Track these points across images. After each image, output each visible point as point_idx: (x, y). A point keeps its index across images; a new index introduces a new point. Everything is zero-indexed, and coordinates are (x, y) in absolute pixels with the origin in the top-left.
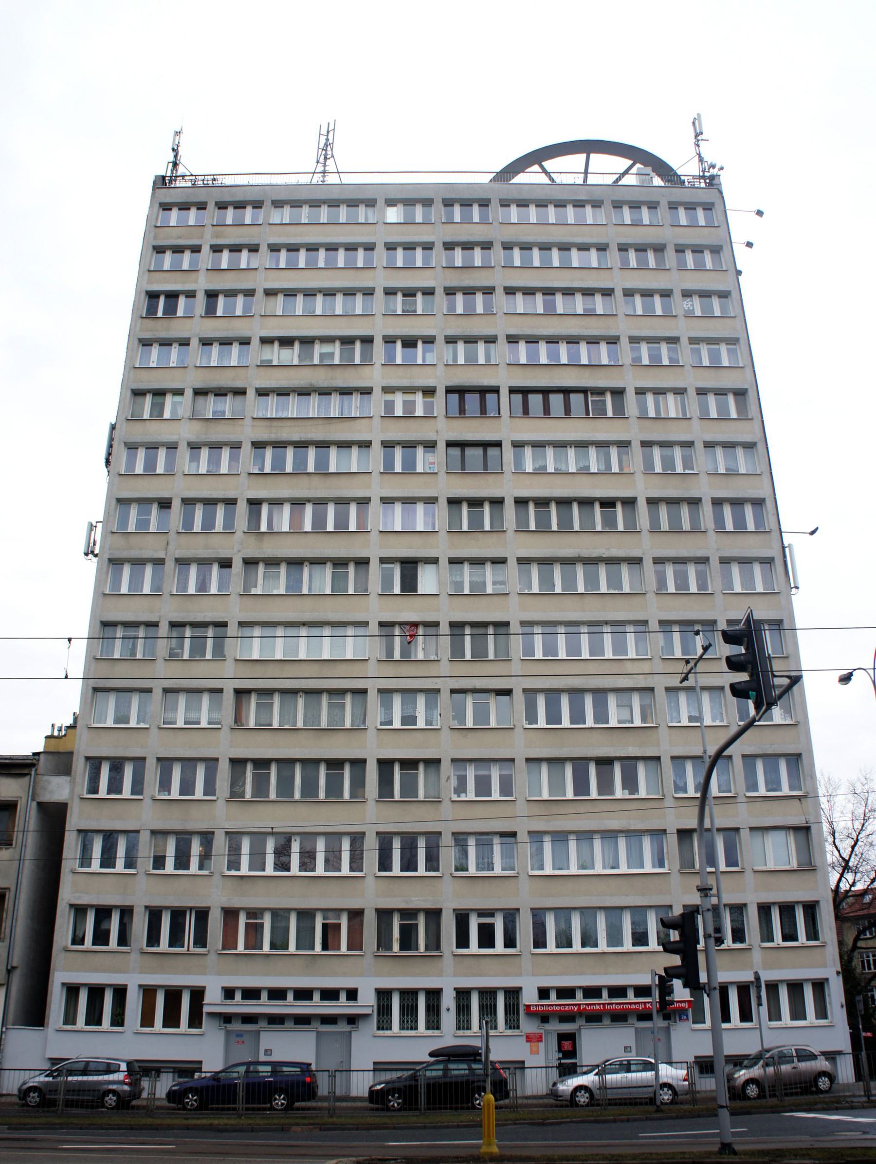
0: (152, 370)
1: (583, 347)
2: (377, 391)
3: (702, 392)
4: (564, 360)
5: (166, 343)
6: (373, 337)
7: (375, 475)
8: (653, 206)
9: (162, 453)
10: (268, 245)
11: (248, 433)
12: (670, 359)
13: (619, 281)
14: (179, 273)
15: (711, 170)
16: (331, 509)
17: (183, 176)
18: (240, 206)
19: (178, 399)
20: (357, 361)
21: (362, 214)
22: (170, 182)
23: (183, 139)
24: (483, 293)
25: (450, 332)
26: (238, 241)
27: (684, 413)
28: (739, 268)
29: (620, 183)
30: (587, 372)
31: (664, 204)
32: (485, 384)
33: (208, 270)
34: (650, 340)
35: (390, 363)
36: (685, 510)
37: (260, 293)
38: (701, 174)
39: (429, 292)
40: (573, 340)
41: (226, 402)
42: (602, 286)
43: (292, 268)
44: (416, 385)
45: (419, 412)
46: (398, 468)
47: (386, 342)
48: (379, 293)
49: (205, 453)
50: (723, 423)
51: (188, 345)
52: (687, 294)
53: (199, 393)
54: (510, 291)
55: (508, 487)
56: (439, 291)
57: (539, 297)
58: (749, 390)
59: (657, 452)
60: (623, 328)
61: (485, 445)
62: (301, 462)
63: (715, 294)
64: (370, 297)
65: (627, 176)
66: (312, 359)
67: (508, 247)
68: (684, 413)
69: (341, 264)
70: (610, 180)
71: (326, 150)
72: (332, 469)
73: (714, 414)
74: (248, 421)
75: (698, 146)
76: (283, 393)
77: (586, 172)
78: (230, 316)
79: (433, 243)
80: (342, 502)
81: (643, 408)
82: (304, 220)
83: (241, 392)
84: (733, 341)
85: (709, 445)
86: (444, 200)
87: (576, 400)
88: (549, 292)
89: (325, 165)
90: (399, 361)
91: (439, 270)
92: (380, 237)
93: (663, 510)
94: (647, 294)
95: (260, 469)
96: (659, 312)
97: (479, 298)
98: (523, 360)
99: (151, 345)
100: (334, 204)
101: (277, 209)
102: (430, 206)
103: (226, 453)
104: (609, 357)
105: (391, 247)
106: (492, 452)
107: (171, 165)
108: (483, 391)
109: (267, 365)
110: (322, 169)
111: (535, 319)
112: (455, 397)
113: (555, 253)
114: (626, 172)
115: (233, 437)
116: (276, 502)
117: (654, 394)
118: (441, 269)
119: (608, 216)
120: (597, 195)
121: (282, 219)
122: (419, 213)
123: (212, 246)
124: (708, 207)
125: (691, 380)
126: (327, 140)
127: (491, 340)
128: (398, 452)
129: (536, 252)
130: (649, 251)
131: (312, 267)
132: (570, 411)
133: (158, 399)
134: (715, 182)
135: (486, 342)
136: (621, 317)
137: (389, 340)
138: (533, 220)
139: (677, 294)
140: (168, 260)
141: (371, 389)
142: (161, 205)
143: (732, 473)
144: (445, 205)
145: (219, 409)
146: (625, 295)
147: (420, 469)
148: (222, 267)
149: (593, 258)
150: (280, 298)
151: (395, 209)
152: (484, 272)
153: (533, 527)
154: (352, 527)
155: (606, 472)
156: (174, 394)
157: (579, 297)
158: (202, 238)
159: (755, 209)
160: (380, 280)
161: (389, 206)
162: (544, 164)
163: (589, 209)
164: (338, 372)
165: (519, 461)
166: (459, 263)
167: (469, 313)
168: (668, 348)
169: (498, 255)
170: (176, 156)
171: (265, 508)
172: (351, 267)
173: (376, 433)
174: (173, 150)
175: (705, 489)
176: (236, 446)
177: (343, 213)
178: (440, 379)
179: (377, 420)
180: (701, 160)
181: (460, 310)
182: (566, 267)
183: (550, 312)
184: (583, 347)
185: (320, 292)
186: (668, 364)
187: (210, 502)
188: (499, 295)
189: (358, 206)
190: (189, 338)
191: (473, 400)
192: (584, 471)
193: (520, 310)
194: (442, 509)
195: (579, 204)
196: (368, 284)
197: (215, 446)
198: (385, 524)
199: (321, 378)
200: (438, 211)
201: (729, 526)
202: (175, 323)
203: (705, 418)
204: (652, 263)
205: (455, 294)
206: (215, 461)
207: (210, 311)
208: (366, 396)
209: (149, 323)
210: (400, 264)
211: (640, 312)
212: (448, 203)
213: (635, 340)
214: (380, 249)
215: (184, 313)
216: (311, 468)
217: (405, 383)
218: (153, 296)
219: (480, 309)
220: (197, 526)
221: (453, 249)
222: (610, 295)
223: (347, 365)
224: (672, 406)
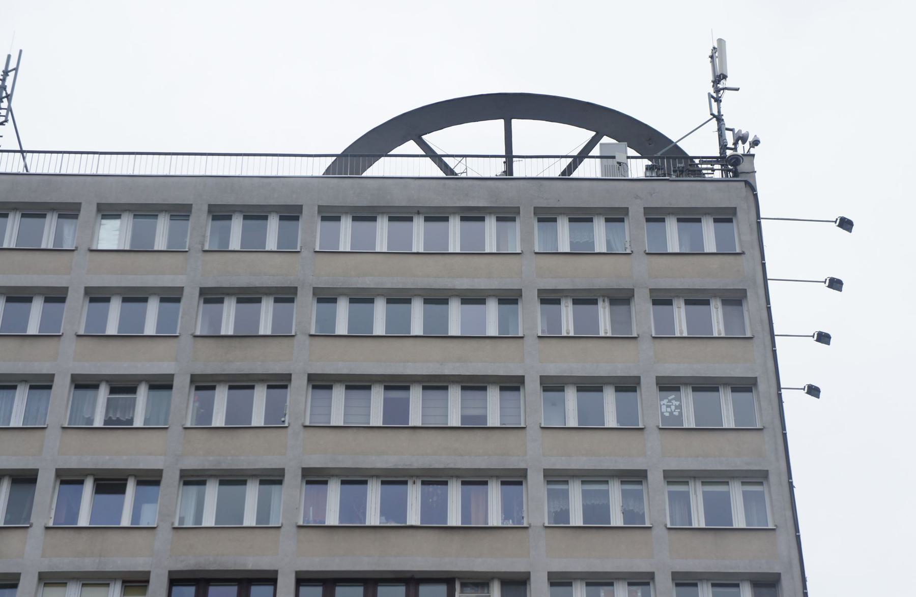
6: (36, 472)
8: (616, 216)
13: (533, 363)
25: (192, 463)
29: (575, 175)
32: (250, 567)
34: (589, 477)
40: (434, 479)
42: (502, 373)
47: (63, 482)
52: (668, 385)
56: (182, 383)
60: (535, 454)
64: (45, 392)
65: (586, 161)
67: (662, 299)
70: (555, 169)
75: (718, 100)
77: (509, 157)
79: (181, 289)
88: (397, 384)
90: (83, 520)
92: (77, 277)
94: (590, 386)
111: (362, 436)
114: (584, 154)
119: (527, 238)
122: (162, 228)
130: (600, 303)
135: (262, 482)
136: (533, 432)
137: (70, 479)
148: (108, 333)
151: (116, 223)
152: (275, 347)
157: (455, 395)
160: (66, 360)
161: (105, 217)
162: (426, 138)
167: (237, 425)
188: (298, 395)
212: (221, 214)
217: (89, 564)
219: (258, 419)
221: (221, 301)
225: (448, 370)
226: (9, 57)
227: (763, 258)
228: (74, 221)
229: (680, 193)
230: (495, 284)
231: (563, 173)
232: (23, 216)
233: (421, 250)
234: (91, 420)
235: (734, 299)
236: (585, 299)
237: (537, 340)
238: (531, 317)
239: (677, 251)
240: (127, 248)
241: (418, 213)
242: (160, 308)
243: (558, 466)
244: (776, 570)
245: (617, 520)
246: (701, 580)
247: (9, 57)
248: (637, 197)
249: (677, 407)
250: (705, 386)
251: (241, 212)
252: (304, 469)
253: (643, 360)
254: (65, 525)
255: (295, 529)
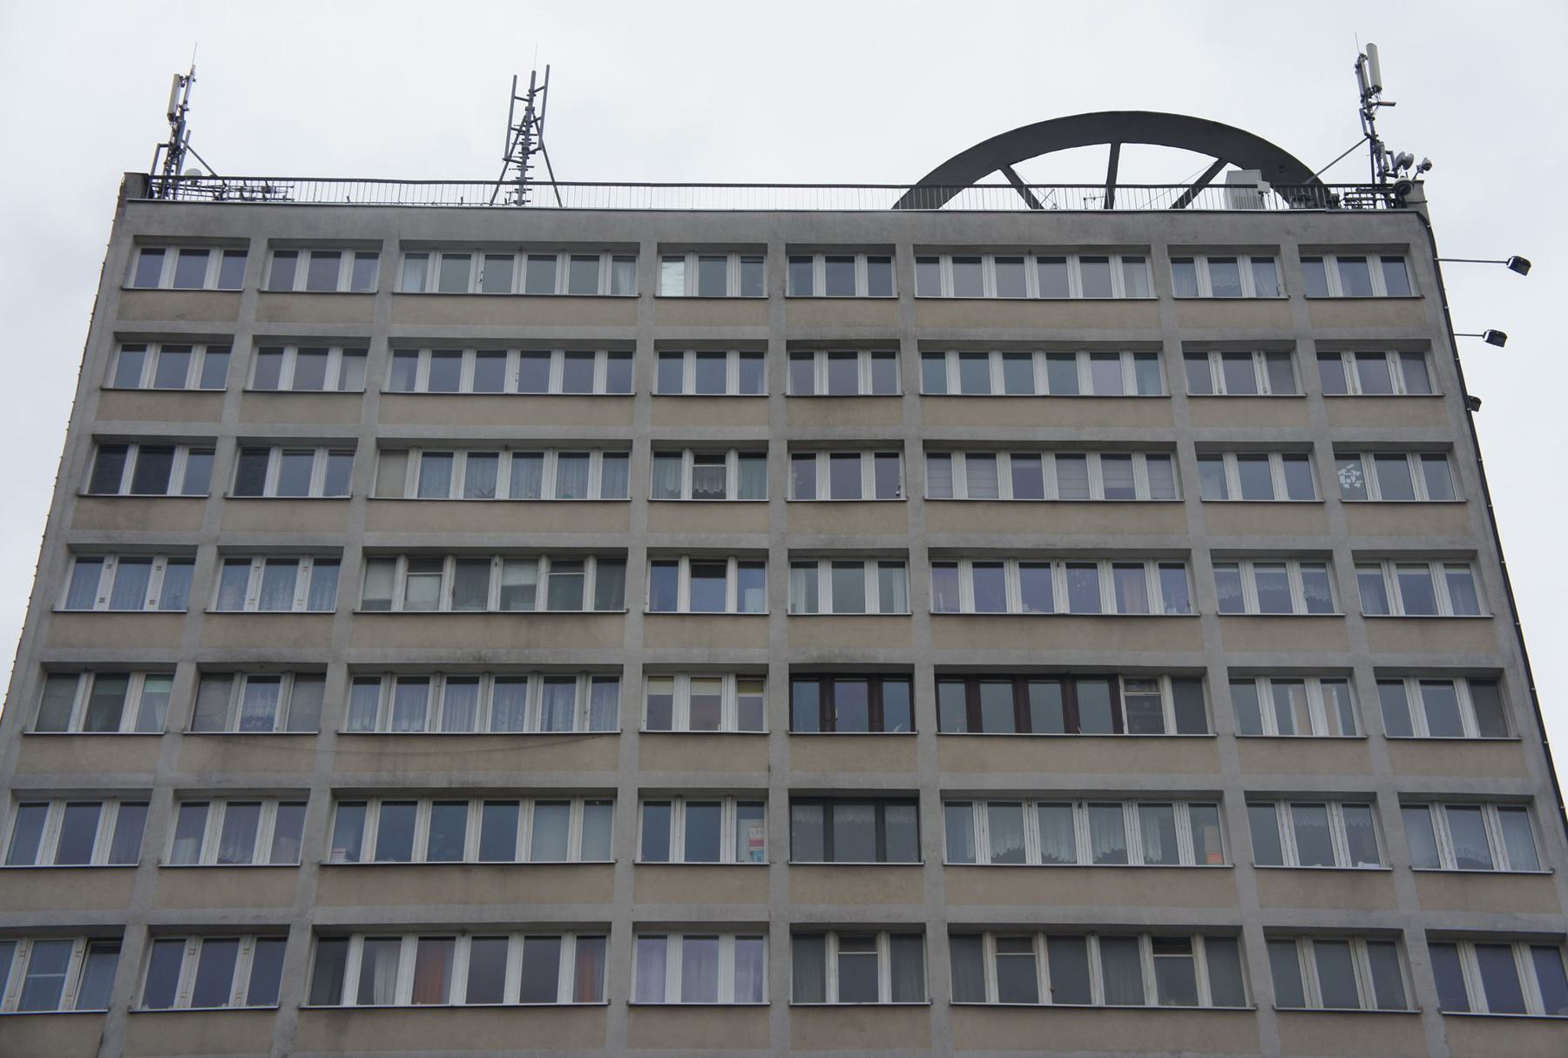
1: (1106, 577)
2: (632, 675)
3: (1389, 677)
4: (1062, 605)
5: (136, 557)
7: (623, 872)
9: (108, 820)
10: (390, 339)
12: (1310, 602)
13: (1187, 427)
14: (177, 397)
15: (1401, 172)
16: (515, 953)
17: (195, 178)
18: (326, 251)
19: (158, 687)
20: (588, 605)
21: (605, 275)
22: (163, 190)
24: (878, 456)
25: (802, 542)
29: (1189, 207)
30: (1116, 632)
31: (1290, 251)
32: (881, 660)
33: (245, 392)
35: (663, 610)
36: (1362, 961)
37: (367, 449)
38: (1378, 181)
39: (754, 452)
40: (1081, 561)
41: (275, 696)
42: (1148, 438)
45: (729, 724)
46: (677, 855)
47: (655, 564)
48: (641, 455)
49: (216, 817)
50: (1446, 750)
51: (192, 562)
52: (1347, 452)
53: (211, 674)
54: (938, 451)
55: (932, 899)
56: (778, 451)
57: (1004, 465)
58: (1507, 673)
59: (1286, 820)
60: (1198, 532)
61: (881, 800)
62: (447, 840)
63: (1414, 452)
64: (620, 461)
66: (484, 600)
67: (933, 351)
68: (1348, 724)
70: (1165, 200)
71: (527, 134)
72: (522, 855)
74: (326, 741)
75: (1370, 118)
76: (413, 676)
77: (1111, 185)
80: (542, 935)
81: (1250, 714)
82: (474, 287)
83: (313, 674)
85: (1413, 802)
86: (790, 248)
87: (1092, 695)
88: (1026, 451)
89: (523, 167)
90: (683, 606)
91: (777, 402)
92: (646, 329)
93: (1308, 961)
94: (1253, 453)
95: (349, 856)
96: (1281, 494)
97: (868, 466)
98: (968, 606)
99: (100, 561)
100: (542, 252)
101: (412, 262)
102: (760, 260)
103: (267, 819)
105: (669, 351)
106: (897, 817)
107: (164, 152)
108: (877, 677)
109: (377, 611)
110: (518, 174)
111: (994, 511)
112: (812, 689)
114: (1204, 182)
116: (384, 936)
117: (1274, 682)
118: (782, 401)
121: (423, 287)
122: (734, 276)
123: (257, 340)
124: (1394, 255)
125: (1363, 650)
126: (530, 110)
127: (894, 560)
128: (678, 820)
129: (996, 364)
130: (1255, 358)
133: (108, 688)
134: (1409, 197)
136: (1193, 507)
137: (663, 560)
138: (991, 291)
139: (1324, 453)
140: (149, 368)
143: (1474, 873)
144: (793, 260)
145: (259, 712)
146: (1200, 458)
147: (727, 856)
149: (1127, 375)
150: (415, 460)
151: (680, 266)
152: (879, 408)
153: (993, 998)
154: (565, 996)
155: (1166, 867)
157: (1094, 464)
158: (235, 319)
159: (1509, 255)
160: (643, 425)
161: (666, 259)
163: (1116, 267)
165: (959, 840)
168: (1305, 576)
170: (177, 133)
171: (355, 953)
173: (628, 769)
174: (172, 117)
175: (1410, 910)
176: (293, 800)
177: (563, 274)
178: (776, 648)
179: (629, 742)
180: (1377, 149)
181: (823, 493)
182: (1064, 396)
185: (507, 448)
186: (1305, 612)
187: (220, 937)
188: (914, 464)
190: (195, 547)
192: (1113, 864)
193: (961, 493)
194: (778, 952)
195: (1094, 256)
197: (244, 801)
198: (643, 988)
199: (503, 644)
200: (776, 273)
201: (1479, 1003)
202: (159, 511)
203: (1400, 738)
204: (1263, 385)
205: (813, 457)
207: (249, 486)
208: (606, 686)
211: (1236, 494)
212: (800, 255)
213: (1225, 559)
216: (471, 854)
217: (698, 656)
218: (109, 449)
219: (869, 492)
220: (184, 996)
222: (1167, 458)
223: (566, 612)
224: (1318, 711)
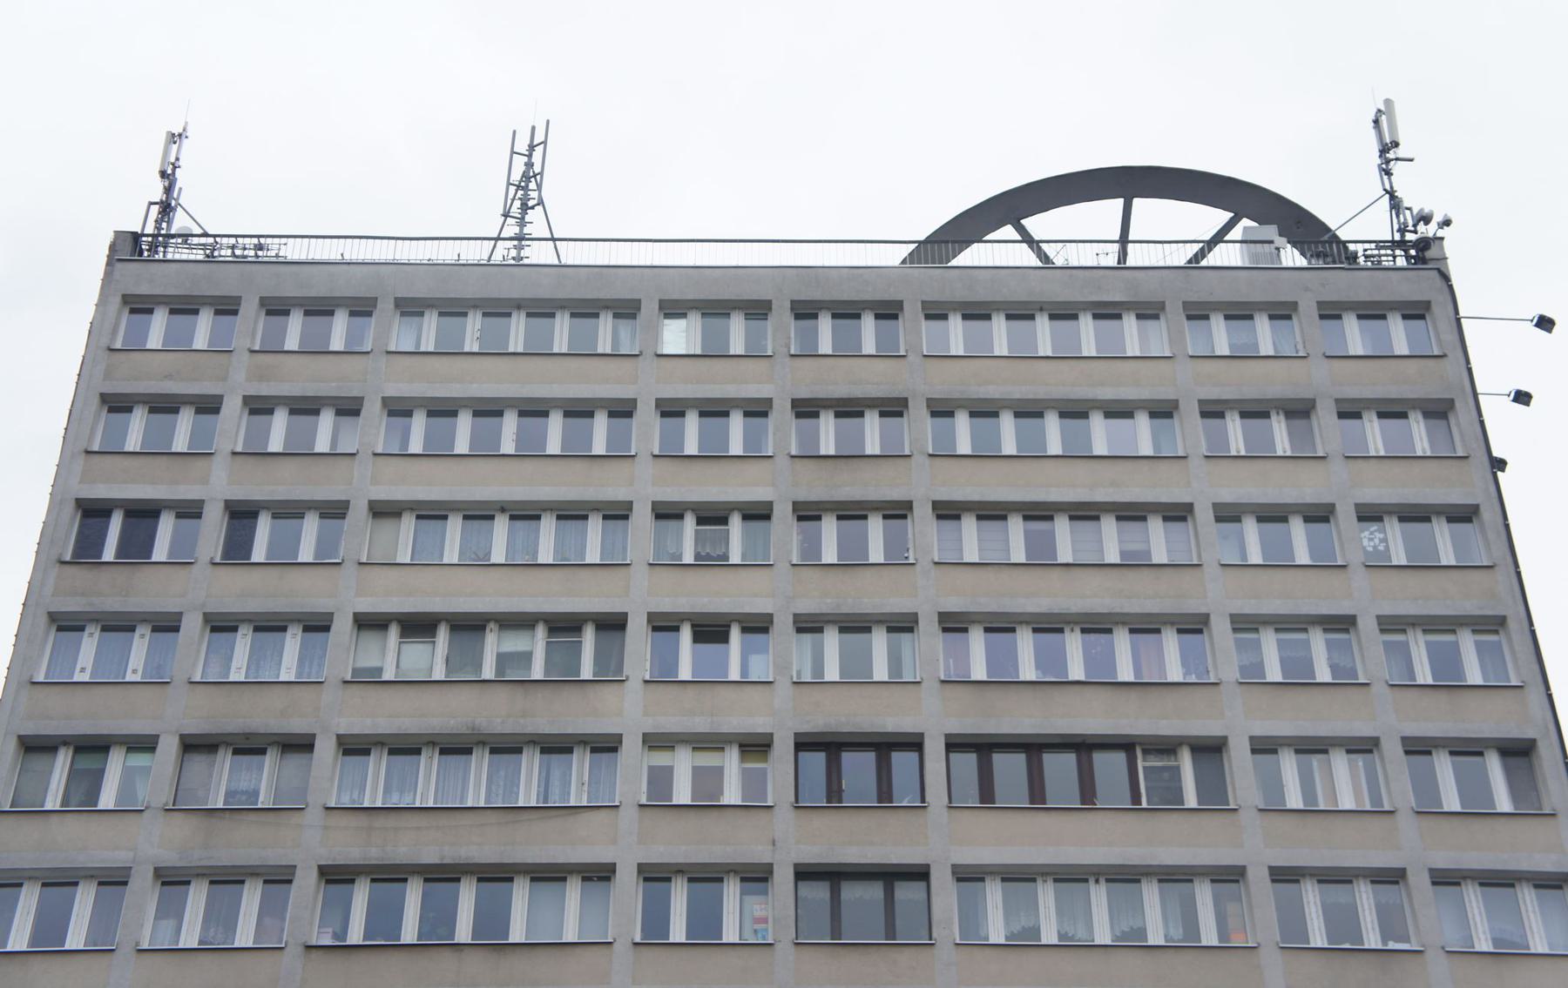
0: (79, 690)
2: (631, 746)
3: (1417, 748)
4: (1076, 672)
5: (119, 625)
8: (1282, 312)
9: (84, 900)
11: (310, 844)
12: (1334, 668)
13: (1204, 488)
15: (1421, 227)
17: (186, 236)
18: (319, 309)
20: (587, 672)
22: (153, 248)
23: (188, 153)
25: (807, 606)
26: (311, 390)
27: (1375, 796)
28: (1496, 453)
29: (1204, 263)
31: (1308, 308)
33: (234, 453)
37: (359, 512)
38: (1397, 237)
39: (758, 514)
40: (1096, 626)
41: (261, 768)
43: (438, 453)
44: (725, 729)
46: (678, 933)
47: (655, 629)
48: (642, 516)
49: (197, 897)
50: (1477, 825)
51: (176, 629)
52: (1369, 514)
53: (194, 746)
54: (948, 512)
56: (783, 512)
59: (1311, 896)
60: (1218, 597)
61: (890, 876)
62: (439, 918)
64: (620, 523)
67: (942, 410)
68: (1375, 796)
69: (554, 447)
70: (1181, 256)
71: (526, 190)
72: (517, 935)
73: (1451, 801)
74: (314, 816)
75: (1388, 173)
76: (405, 747)
77: (1124, 240)
78: (283, 562)
79: (769, 401)
81: (1274, 786)
82: (471, 345)
83: (300, 745)
84: (1491, 625)
85: (1445, 879)
88: (1038, 513)
89: (522, 223)
90: (685, 673)
91: (782, 462)
92: (646, 387)
94: (1272, 515)
95: (335, 936)
96: (1302, 557)
97: (875, 527)
100: (541, 310)
102: (764, 317)
103: (251, 897)
104: (1185, 663)
105: (671, 410)
106: (907, 892)
107: (155, 209)
108: (884, 746)
109: (368, 680)
110: (517, 230)
111: (1006, 574)
112: (817, 760)
113: (1052, 423)
114: (1218, 238)
115: (273, 856)
117: (1297, 752)
118: (787, 461)
119: (1176, 338)
120: (1148, 291)
121: (418, 344)
122: (737, 333)
123: (247, 400)
125: (1391, 719)
126: (529, 165)
129: (1007, 422)
130: (1274, 417)
131: (485, 452)
132: (1094, 795)
133: (88, 762)
136: (1211, 570)
137: (664, 625)
139: (1345, 515)
141: (618, 738)
142: (126, 299)
144: (798, 317)
146: (1219, 519)
147: (730, 935)
148: (271, 449)
149: (1142, 434)
150: (408, 523)
151: (682, 323)
152: (888, 468)
156: (130, 750)
158: (224, 379)
160: (643, 485)
161: (668, 316)
164: (540, 697)
165: (971, 917)
166: (828, 447)
168: (1328, 643)
169: (919, 428)
170: (168, 190)
172: (576, 454)
173: (626, 843)
174: (163, 174)
176: (279, 878)
178: (780, 717)
179: (629, 815)
180: (1396, 204)
181: (830, 555)
183: (1041, 561)
184: (1122, 642)
185: (503, 510)
188: (923, 522)
189: (596, 316)
191: (859, 766)
193: (971, 555)
195: (1107, 312)
196: (614, 492)
197: (227, 879)
200: (781, 330)
203: (1429, 811)
204: (1282, 445)
205: (819, 518)
206: (221, 916)
207: (237, 550)
208: (605, 756)
209: (80, 576)
210: (691, 448)
211: (1255, 557)
212: (805, 311)
213: (1245, 624)
214: (646, 414)
215: (170, 554)
217: (701, 725)
218: (93, 513)
219: (876, 554)
221: (816, 415)
222: (1184, 519)
223: (563, 680)
225: (1100, 496)
226: (533, 128)
227: (1468, 362)
228: (630, 321)
229: (1340, 284)
230: (1145, 394)
231: (1190, 261)
232: (441, 314)
233: (520, 350)
234: (680, 557)
235: (1438, 411)
236: (1255, 411)
237: (1204, 461)
238: (1190, 432)
239: (1138, 354)
240: (699, 352)
241: (1041, 310)
242: (518, 426)
243: (1247, 611)
244: (1530, 734)
245: (1323, 674)
246: (1436, 747)
247: (533, 128)
248: (1307, 289)
249: (1381, 541)
250: (1414, 515)
251: (347, 306)
252: (941, 614)
253: (1341, 486)
254: (664, 678)
255: (938, 685)
